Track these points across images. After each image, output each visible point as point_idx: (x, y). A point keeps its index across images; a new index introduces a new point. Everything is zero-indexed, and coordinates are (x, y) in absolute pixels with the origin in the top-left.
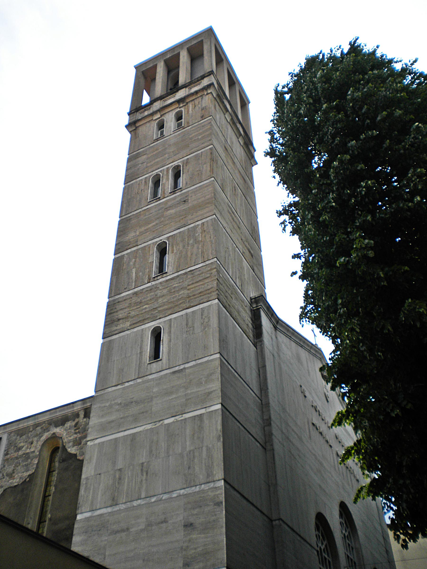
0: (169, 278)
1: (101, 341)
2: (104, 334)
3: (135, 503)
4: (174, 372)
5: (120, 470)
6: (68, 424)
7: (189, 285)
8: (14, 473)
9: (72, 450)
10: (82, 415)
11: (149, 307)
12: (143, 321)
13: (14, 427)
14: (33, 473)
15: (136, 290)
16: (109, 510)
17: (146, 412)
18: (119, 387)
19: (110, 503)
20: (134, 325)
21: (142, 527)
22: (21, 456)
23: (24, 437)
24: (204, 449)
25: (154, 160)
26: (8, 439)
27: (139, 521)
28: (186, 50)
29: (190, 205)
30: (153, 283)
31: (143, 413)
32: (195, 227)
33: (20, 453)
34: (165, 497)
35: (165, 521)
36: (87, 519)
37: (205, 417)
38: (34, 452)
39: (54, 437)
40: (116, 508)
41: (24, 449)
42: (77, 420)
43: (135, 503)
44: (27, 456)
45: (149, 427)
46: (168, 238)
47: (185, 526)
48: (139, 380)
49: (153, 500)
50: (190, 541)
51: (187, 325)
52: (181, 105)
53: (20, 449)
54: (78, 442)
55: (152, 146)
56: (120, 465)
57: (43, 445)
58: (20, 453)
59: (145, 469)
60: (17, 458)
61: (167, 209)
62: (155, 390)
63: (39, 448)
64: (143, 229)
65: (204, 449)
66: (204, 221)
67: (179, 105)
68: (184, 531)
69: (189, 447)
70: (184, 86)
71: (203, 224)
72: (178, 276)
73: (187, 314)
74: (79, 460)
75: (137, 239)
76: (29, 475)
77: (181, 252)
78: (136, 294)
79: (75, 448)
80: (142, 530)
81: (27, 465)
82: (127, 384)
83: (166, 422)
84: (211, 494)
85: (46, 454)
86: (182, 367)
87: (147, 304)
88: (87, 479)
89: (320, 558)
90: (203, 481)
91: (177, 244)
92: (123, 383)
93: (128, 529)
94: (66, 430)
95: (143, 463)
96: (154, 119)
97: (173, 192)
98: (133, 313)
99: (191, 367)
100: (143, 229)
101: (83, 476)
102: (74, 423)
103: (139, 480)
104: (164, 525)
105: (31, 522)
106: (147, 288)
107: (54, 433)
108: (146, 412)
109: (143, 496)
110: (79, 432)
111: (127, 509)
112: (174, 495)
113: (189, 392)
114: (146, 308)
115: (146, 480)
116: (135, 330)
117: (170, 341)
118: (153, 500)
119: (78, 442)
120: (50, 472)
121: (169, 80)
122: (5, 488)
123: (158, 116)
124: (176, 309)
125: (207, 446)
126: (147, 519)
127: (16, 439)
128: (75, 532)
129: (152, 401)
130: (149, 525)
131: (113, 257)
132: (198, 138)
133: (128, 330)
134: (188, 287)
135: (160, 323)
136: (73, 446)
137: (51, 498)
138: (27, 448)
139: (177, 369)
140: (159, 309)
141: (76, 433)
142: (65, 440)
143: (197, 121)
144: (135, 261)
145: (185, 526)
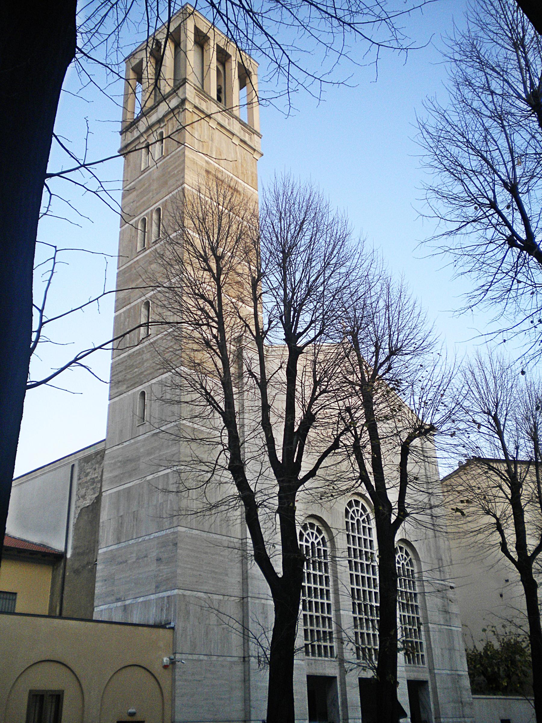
1: (108, 402)
2: (110, 395)
3: (131, 542)
5: (121, 516)
8: (86, 495)
11: (138, 371)
13: (81, 455)
17: (136, 469)
18: (120, 446)
19: (116, 542)
21: (134, 560)
23: (89, 463)
24: (169, 502)
25: (141, 199)
26: (79, 465)
27: (132, 555)
31: (134, 470)
33: (89, 478)
34: (147, 538)
36: (105, 553)
38: (97, 477)
41: (90, 474)
45: (138, 482)
48: (132, 441)
50: (159, 570)
52: (162, 125)
53: (87, 475)
58: (89, 478)
60: (86, 482)
62: (142, 450)
65: (169, 502)
67: (160, 124)
68: (157, 563)
69: (160, 501)
75: (130, 296)
76: (96, 497)
80: (134, 562)
81: (93, 489)
82: (125, 444)
83: (149, 478)
87: (137, 368)
88: (103, 522)
90: (167, 527)
93: (126, 561)
95: (134, 512)
96: (141, 142)
98: (129, 376)
101: (101, 521)
103: (132, 525)
106: (136, 351)
108: (136, 469)
112: (152, 537)
114: (136, 372)
115: (136, 525)
118: (140, 540)
125: (170, 500)
126: (137, 554)
127: (84, 466)
129: (139, 460)
130: (138, 559)
131: (113, 315)
132: (174, 174)
133: (125, 392)
138: (92, 474)
140: (145, 373)
143: (174, 150)
145: (157, 560)
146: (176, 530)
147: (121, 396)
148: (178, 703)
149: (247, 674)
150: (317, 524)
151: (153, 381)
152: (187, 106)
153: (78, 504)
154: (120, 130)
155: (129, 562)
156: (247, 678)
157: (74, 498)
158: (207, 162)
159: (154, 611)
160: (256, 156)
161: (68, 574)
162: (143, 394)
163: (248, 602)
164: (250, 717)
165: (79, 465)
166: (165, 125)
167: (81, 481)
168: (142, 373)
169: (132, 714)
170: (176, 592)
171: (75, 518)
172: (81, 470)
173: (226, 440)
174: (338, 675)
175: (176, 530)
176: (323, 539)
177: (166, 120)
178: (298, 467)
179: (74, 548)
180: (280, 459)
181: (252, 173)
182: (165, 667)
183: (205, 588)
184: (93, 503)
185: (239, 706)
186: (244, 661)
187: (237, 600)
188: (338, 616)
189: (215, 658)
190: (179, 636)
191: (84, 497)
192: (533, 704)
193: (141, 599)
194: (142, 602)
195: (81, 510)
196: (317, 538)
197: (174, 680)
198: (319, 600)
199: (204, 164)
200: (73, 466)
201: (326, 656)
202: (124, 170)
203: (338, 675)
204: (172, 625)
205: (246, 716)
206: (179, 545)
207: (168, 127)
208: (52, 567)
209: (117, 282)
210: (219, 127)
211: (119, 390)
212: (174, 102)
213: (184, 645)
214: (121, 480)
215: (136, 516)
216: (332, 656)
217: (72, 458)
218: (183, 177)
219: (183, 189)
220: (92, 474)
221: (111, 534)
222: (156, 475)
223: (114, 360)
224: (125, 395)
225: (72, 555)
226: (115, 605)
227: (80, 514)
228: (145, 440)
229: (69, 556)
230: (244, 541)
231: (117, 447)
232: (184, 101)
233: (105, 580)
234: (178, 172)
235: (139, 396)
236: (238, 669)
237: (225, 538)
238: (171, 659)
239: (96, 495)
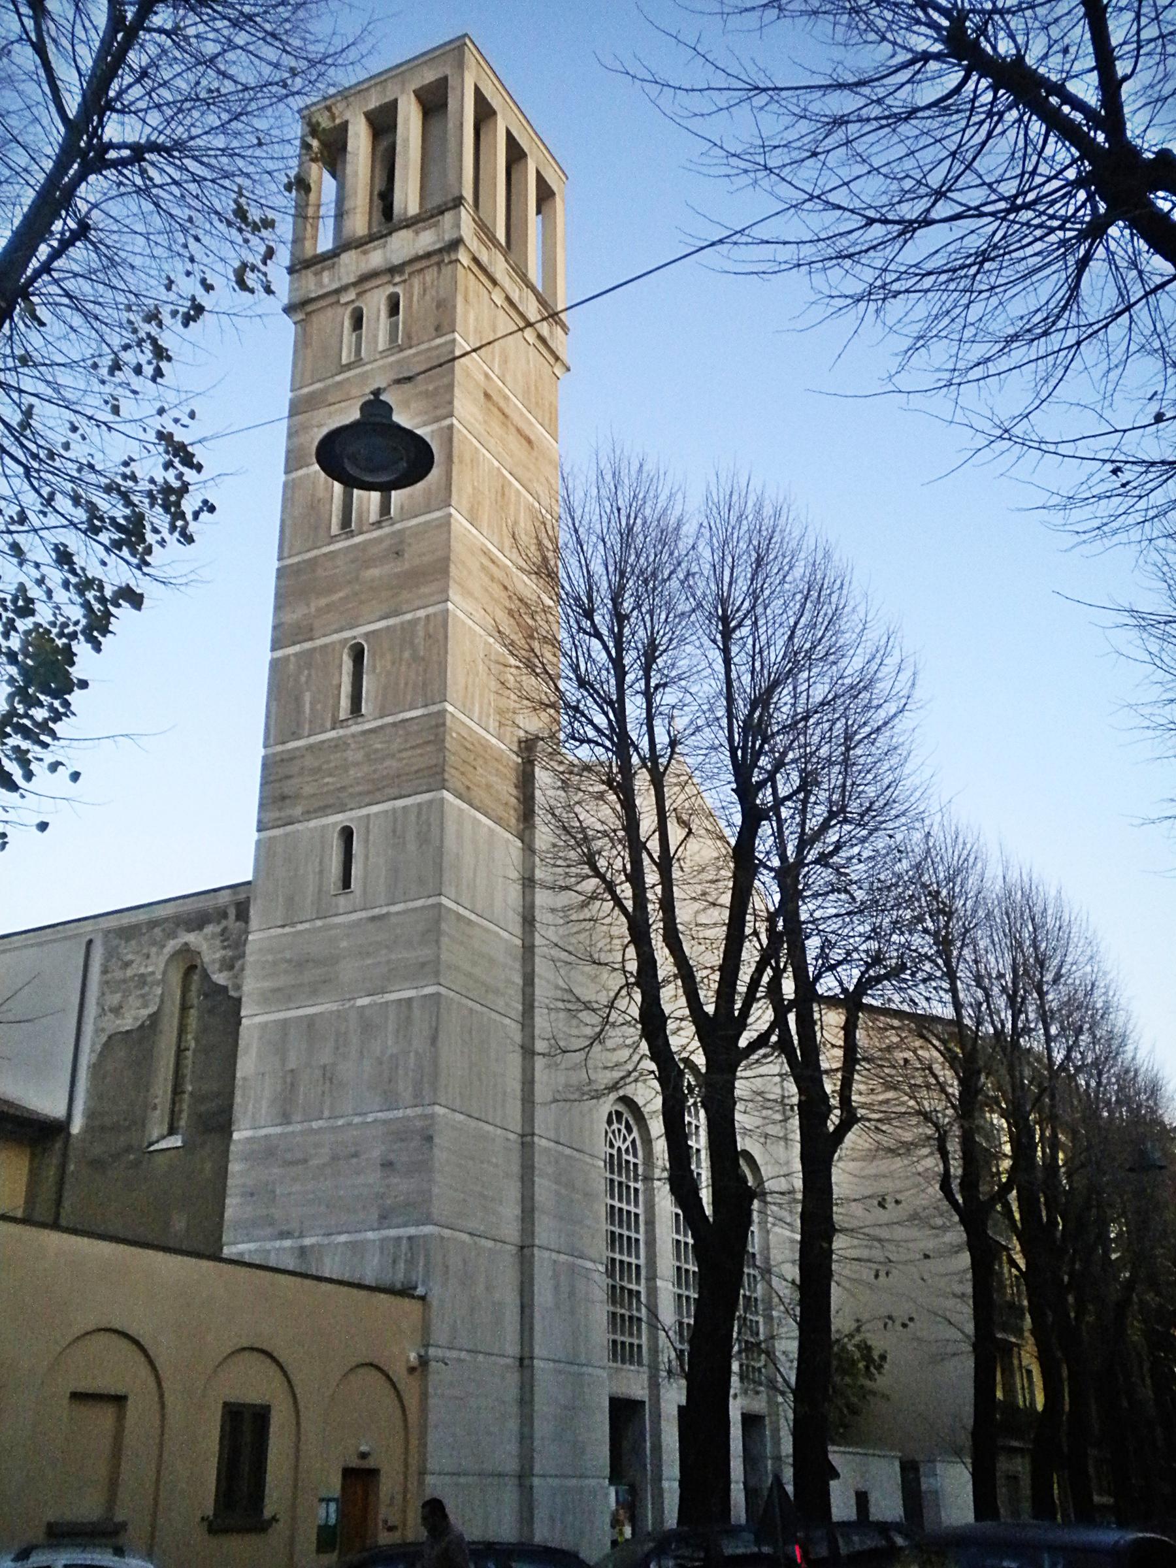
0: (367, 726)
2: (259, 822)
4: (373, 919)
6: (209, 929)
7: (400, 751)
9: (220, 978)
10: (232, 912)
12: (324, 810)
13: (113, 922)
14: (155, 1013)
15: (313, 740)
16: (278, 1130)
18: (287, 930)
20: (309, 814)
21: (326, 1159)
22: (132, 978)
23: (133, 943)
28: (412, 96)
29: (407, 566)
30: (341, 732)
32: (415, 622)
33: (129, 972)
34: (357, 1120)
35: (355, 1155)
36: (249, 1140)
37: (415, 1004)
38: (153, 973)
39: (186, 949)
40: (290, 1129)
42: (224, 923)
43: (315, 1125)
44: (142, 980)
45: (334, 1007)
46: (367, 635)
47: (382, 1165)
48: (319, 923)
49: (340, 1122)
51: (394, 831)
53: (127, 964)
54: (228, 965)
55: (339, 383)
56: (291, 1065)
57: (167, 964)
58: (129, 972)
59: (328, 1075)
60: (124, 981)
61: (368, 563)
62: (344, 944)
63: (162, 966)
64: (323, 602)
66: (431, 610)
69: (393, 1049)
70: (411, 223)
71: (428, 617)
72: (381, 727)
73: (394, 810)
74: (230, 997)
76: (150, 1016)
77: (388, 674)
78: (310, 748)
79: (225, 974)
81: (143, 996)
82: (300, 927)
83: (360, 1002)
84: (419, 1124)
85: (175, 978)
86: (384, 910)
87: (330, 775)
89: (700, 1142)
91: (382, 656)
92: (293, 924)
93: (306, 1161)
94: (206, 939)
96: (343, 301)
97: (378, 524)
99: (398, 913)
100: (323, 602)
101: (238, 1075)
102: (218, 929)
104: (354, 1160)
105: (160, 1093)
107: (186, 944)
109: (326, 1114)
110: (229, 946)
111: (302, 1133)
113: (393, 957)
116: (313, 824)
117: (367, 857)
118: (340, 1122)
119: (228, 965)
120: (184, 1008)
121: (377, 171)
122: (108, 1033)
123: (351, 295)
124: (378, 796)
128: (231, 1157)
130: (335, 1158)
134: (398, 756)
135: (351, 820)
136: (221, 971)
137: (189, 1054)
139: (376, 911)
140: (351, 790)
141: (224, 948)
142: (206, 959)
144: (309, 675)
145: (382, 1165)
146: (429, 1110)
147: (289, 828)
148: (433, 1437)
149: (527, 1388)
150: (627, 1115)
151: (375, 809)
152: (463, 257)
153: (101, 1025)
154: (287, 263)
155: (314, 1162)
156: (527, 1398)
157: (91, 1010)
158: (487, 376)
159: (376, 1261)
160: (558, 370)
161: (72, 1167)
162: (347, 834)
163: (533, 1255)
164: (532, 1468)
165: (106, 943)
166: (404, 281)
167: (109, 976)
168: (343, 788)
169: (364, 1456)
170: (428, 1229)
171: (92, 1051)
172: (110, 954)
173: (632, 966)
174: (647, 1399)
175: (429, 1110)
176: (633, 1141)
177: (408, 270)
178: (741, 1023)
179: (90, 1115)
180: (710, 1009)
181: (551, 404)
182: (412, 1370)
183: (471, 1225)
184: (142, 1026)
185: (512, 1447)
186: (521, 1365)
187: (513, 1249)
188: (653, 1291)
189: (481, 1357)
190: (433, 1314)
191: (117, 1011)
192: (970, 1467)
193: (343, 1238)
194: (346, 1243)
195: (110, 1037)
196: (625, 1139)
197: (424, 1396)
198: (626, 1258)
199: (482, 378)
200: (90, 942)
201: (631, 1363)
202: (295, 352)
203: (647, 1399)
204: (420, 1291)
205: (522, 1467)
206: (437, 1140)
207: (411, 286)
208: (28, 1151)
209: (277, 588)
210: (506, 305)
211: (283, 814)
212: (426, 240)
213: (440, 1333)
214: (289, 998)
215: (328, 1075)
216: (640, 1363)
217: (88, 926)
218: (451, 402)
219: (451, 427)
220: (140, 965)
221: (264, 1104)
222: (379, 999)
223: (271, 751)
224: (298, 826)
225: (88, 1129)
226: (277, 1244)
227: (106, 1045)
228: (358, 923)
229: (76, 1128)
230: (528, 1139)
231: (280, 931)
232: (456, 244)
233: (252, 1195)
234: (436, 389)
235: (336, 835)
236: (513, 1379)
237: (499, 1131)
238: (420, 1357)
239: (152, 1009)
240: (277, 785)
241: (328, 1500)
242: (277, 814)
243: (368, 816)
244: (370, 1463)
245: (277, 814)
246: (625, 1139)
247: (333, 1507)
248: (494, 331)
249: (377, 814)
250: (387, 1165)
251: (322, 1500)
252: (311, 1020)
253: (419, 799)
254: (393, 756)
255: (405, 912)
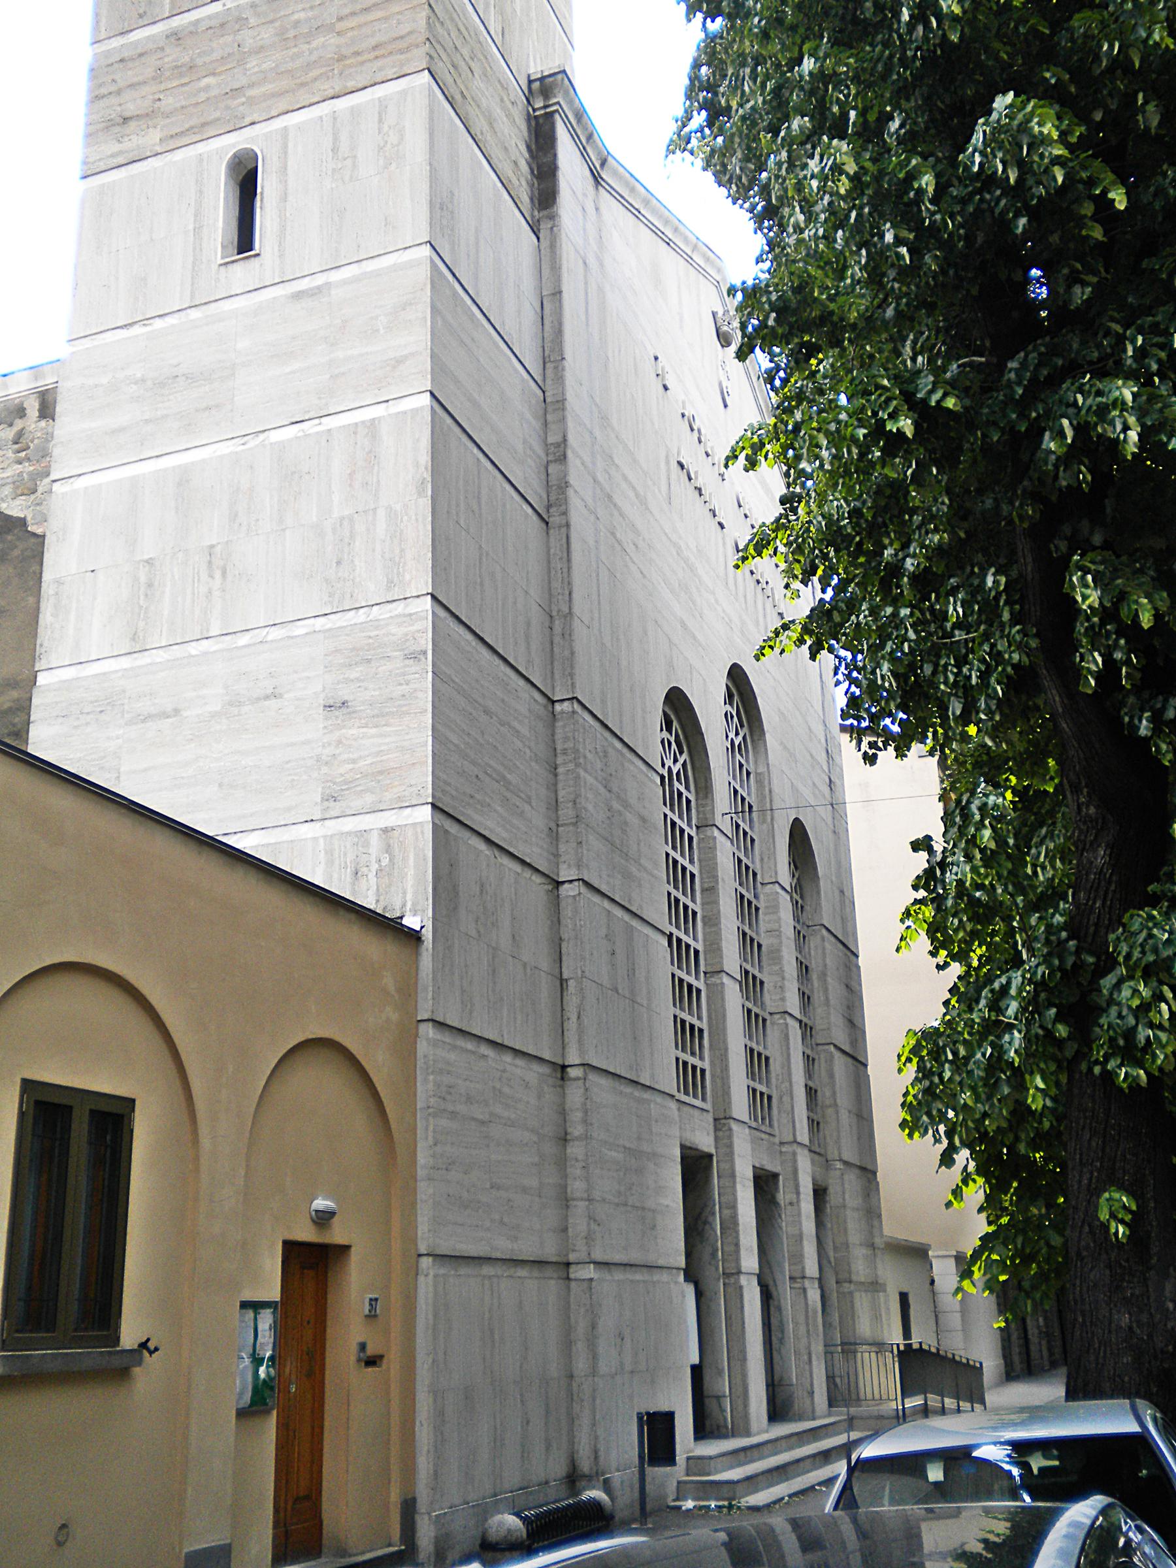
4: (298, 296)
40: (143, 660)
42: (19, 424)
79: (21, 500)
93: (177, 711)
99: (345, 282)
104: (273, 703)
124: (304, 97)
134: (340, 26)
176: (684, 765)
203: (713, 1151)
240: (114, 100)
241: (256, 1306)
242: (115, 147)
243: (286, 128)
244: (337, 1235)
245: (115, 147)
246: (676, 761)
247: (266, 1320)
248: (208, 631)
249: (299, 127)
250: (336, 707)
251: (245, 1305)
252: (183, 477)
253: (380, 91)
254: (330, 28)
255: (356, 280)
